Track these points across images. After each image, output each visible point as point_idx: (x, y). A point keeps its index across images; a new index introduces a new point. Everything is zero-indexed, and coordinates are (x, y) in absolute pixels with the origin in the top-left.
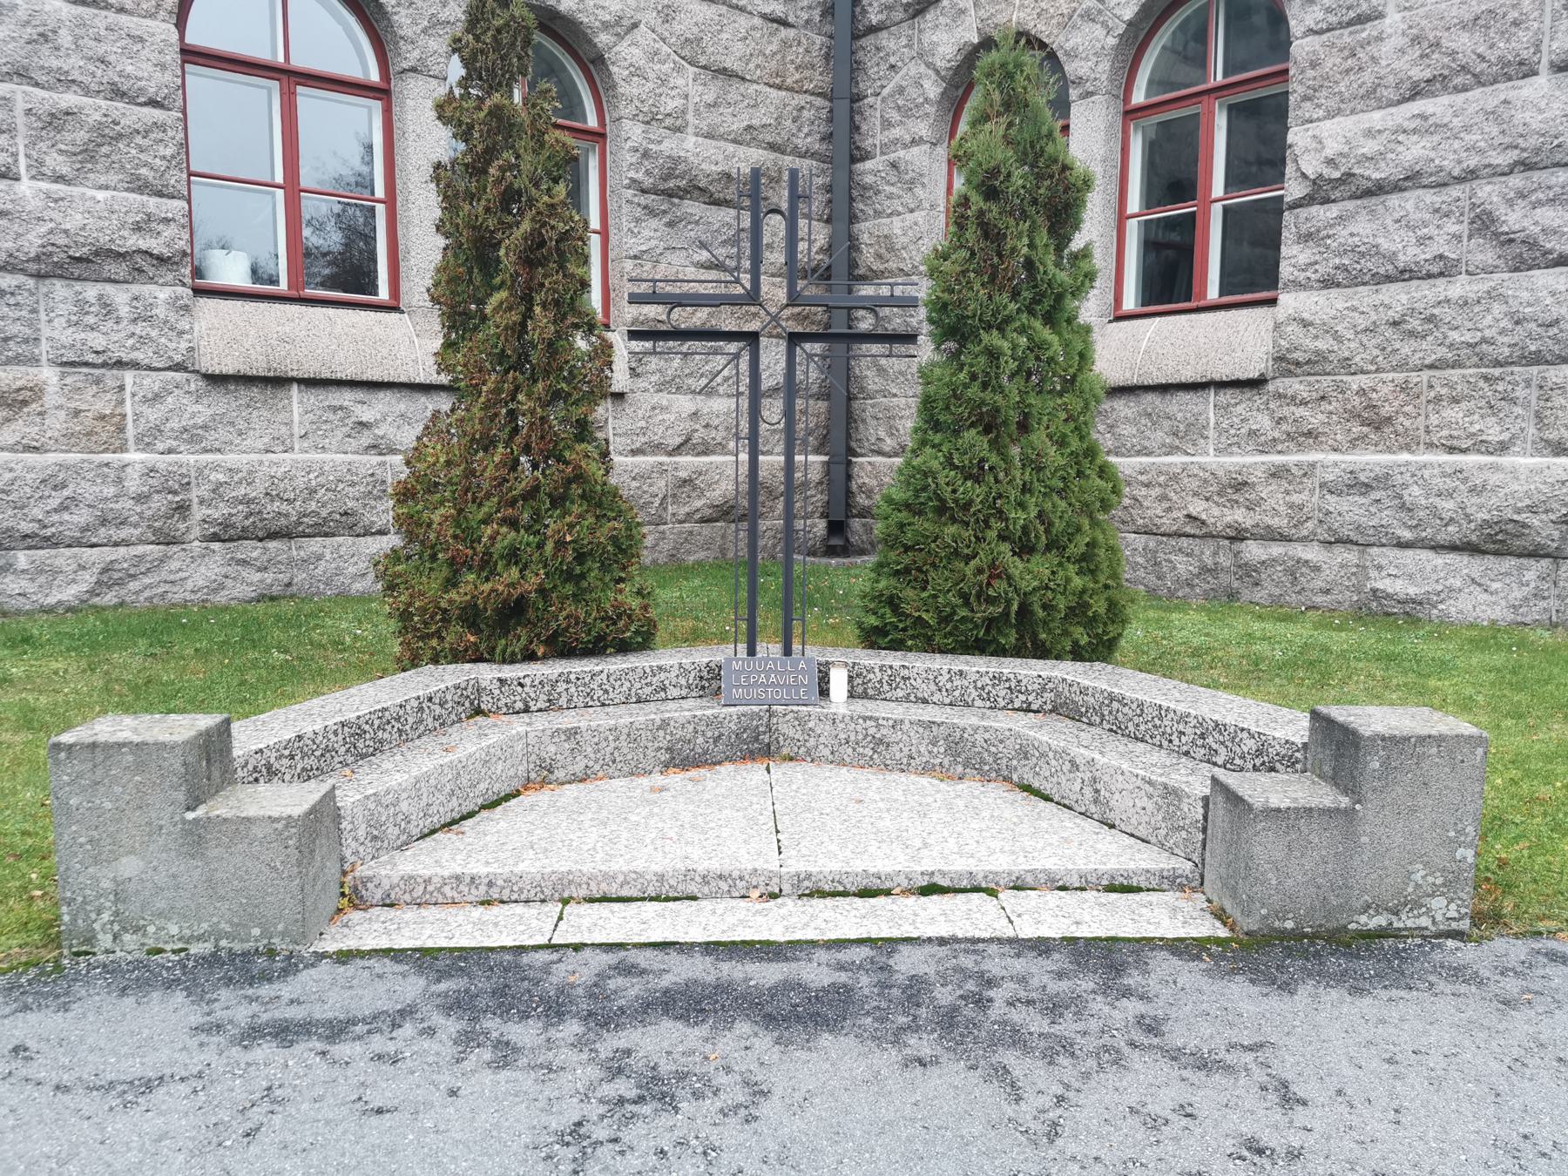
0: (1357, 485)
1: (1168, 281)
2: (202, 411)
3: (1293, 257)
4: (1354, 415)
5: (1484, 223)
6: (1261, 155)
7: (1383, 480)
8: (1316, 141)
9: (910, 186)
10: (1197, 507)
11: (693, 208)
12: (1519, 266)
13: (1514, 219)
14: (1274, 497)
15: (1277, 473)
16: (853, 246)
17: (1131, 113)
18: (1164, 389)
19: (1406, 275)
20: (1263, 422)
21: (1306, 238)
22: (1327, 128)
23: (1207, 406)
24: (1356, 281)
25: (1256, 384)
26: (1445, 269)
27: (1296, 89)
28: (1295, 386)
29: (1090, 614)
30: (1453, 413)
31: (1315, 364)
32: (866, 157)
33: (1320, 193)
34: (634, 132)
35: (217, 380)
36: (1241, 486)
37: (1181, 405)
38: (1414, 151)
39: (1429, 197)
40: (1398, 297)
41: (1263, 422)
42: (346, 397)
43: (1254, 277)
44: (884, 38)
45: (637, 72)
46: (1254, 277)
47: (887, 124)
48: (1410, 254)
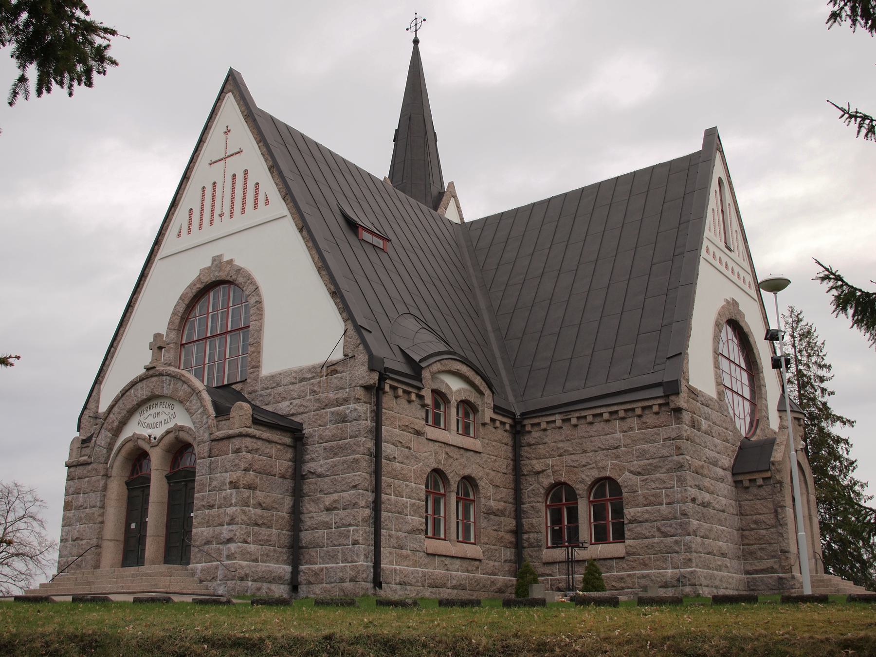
0: (643, 577)
1: (601, 537)
2: (427, 560)
3: (627, 534)
4: (641, 564)
5: (659, 529)
6: (618, 512)
7: (648, 575)
8: (630, 512)
9: (537, 512)
10: (614, 584)
11: (492, 517)
12: (665, 537)
13: (663, 529)
14: (628, 580)
15: (629, 575)
16: (522, 525)
17: (590, 502)
18: (605, 559)
19: (647, 538)
20: (625, 565)
21: (629, 530)
22: (631, 510)
23: (614, 563)
24: (639, 538)
25: (623, 558)
26: (654, 537)
27: (624, 503)
28: (631, 558)
29: (851, 311)
30: (658, 563)
31: (634, 554)
32: (524, 504)
33: (631, 522)
34: (483, 500)
35: (428, 554)
36: (622, 579)
37: (608, 563)
38: (646, 516)
39: (650, 524)
40: (646, 541)
41: (625, 565)
42: (443, 559)
43: (620, 536)
44: (528, 477)
45: (484, 488)
46: (620, 536)
47: (529, 497)
48: (647, 534)
